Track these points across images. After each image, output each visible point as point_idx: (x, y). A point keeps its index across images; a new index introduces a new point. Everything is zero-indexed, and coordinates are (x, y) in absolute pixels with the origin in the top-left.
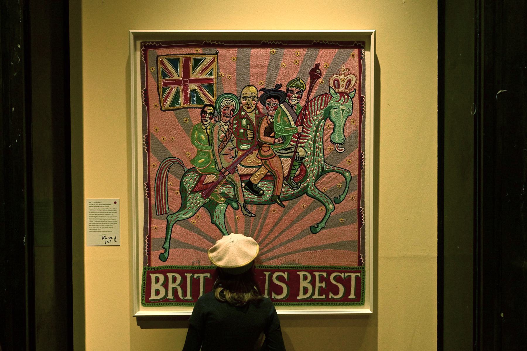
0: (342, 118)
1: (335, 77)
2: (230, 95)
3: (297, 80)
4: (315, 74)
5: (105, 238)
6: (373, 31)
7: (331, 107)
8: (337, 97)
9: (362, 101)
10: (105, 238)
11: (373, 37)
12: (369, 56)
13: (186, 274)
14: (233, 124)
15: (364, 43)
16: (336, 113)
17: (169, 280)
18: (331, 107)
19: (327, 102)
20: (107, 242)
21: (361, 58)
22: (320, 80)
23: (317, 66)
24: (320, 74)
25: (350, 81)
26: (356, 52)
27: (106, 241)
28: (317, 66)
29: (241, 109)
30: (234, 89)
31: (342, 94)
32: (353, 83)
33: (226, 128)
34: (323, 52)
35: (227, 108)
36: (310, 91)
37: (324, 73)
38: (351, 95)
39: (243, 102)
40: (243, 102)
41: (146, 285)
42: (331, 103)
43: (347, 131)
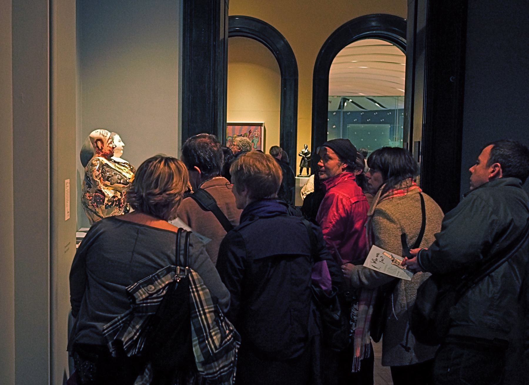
0: (256, 142)
1: (255, 133)
2: (230, 136)
3: (246, 133)
4: (250, 132)
5: (375, 261)
6: (263, 122)
7: (254, 140)
8: (255, 137)
9: (261, 138)
10: (375, 261)
11: (263, 124)
12: (263, 128)
13: (134, 210)
14: (231, 143)
15: (262, 125)
16: (255, 141)
17: (221, 16)
18: (254, 140)
19: (253, 138)
20: (382, 260)
21: (261, 128)
22: (251, 134)
23: (251, 130)
24: (251, 132)
25: (258, 134)
26: (260, 127)
27: (380, 262)
28: (251, 130)
29: (233, 140)
30: (231, 135)
31: (256, 137)
32: (259, 134)
33: (229, 144)
34: (252, 127)
35: (230, 140)
36: (249, 136)
37: (252, 132)
38: (259, 137)
39: (233, 138)
40: (233, 138)
41: (65, 184)
42: (254, 139)
43: (257, 146)
